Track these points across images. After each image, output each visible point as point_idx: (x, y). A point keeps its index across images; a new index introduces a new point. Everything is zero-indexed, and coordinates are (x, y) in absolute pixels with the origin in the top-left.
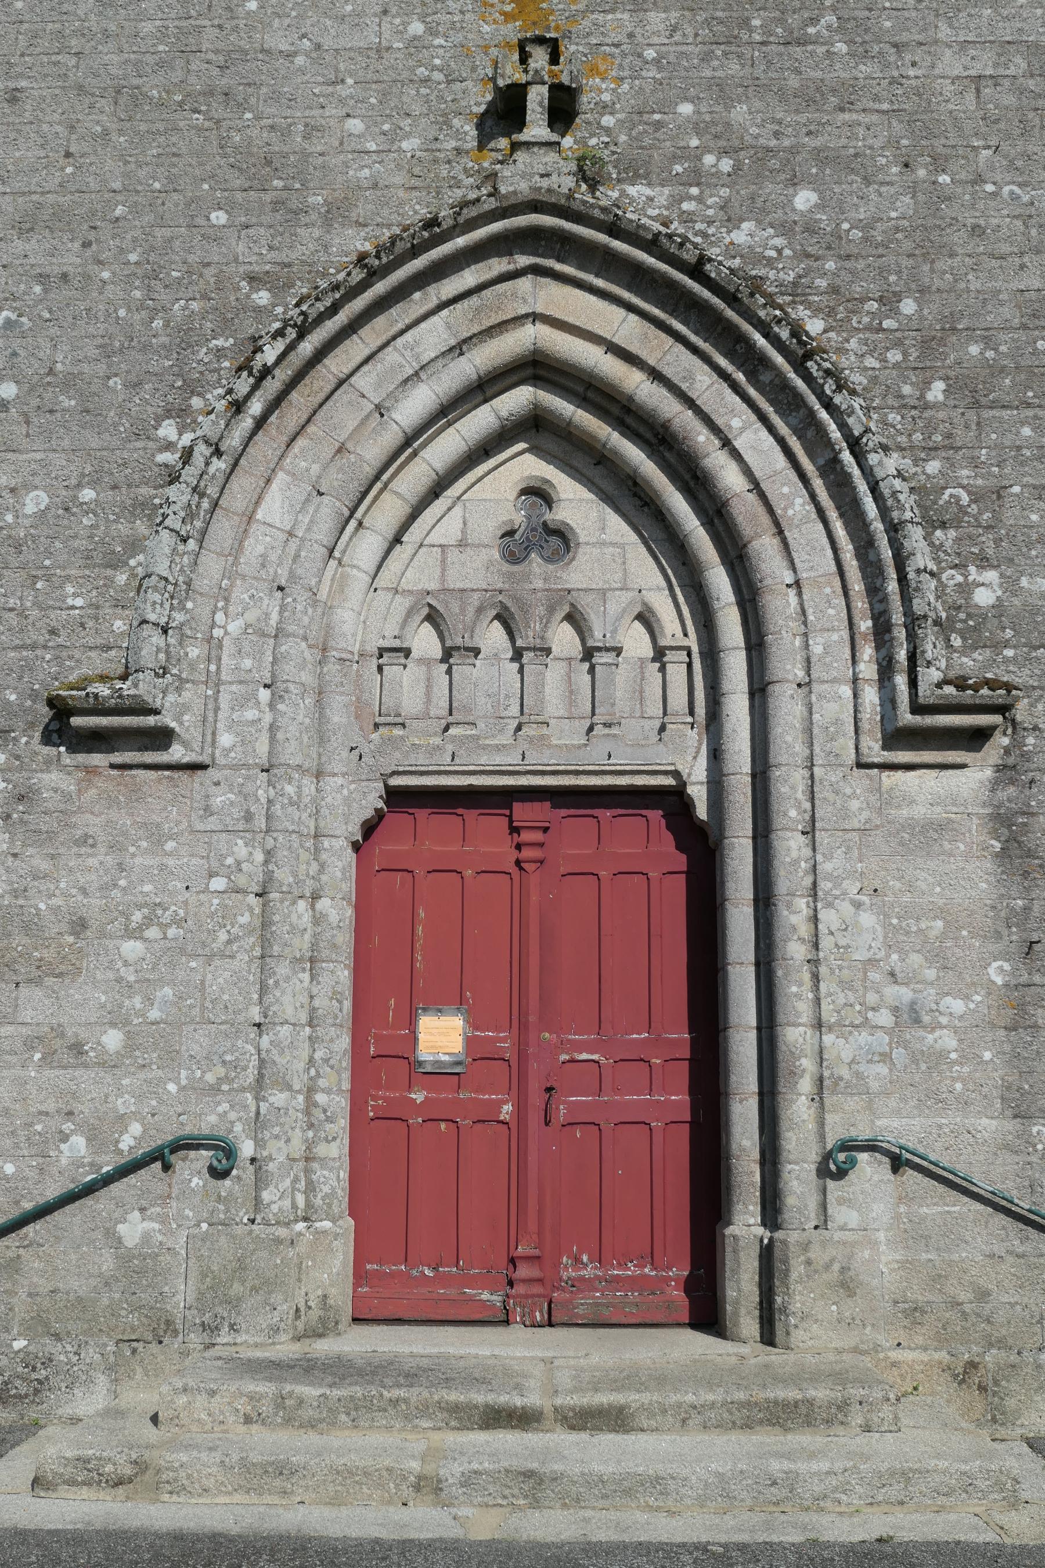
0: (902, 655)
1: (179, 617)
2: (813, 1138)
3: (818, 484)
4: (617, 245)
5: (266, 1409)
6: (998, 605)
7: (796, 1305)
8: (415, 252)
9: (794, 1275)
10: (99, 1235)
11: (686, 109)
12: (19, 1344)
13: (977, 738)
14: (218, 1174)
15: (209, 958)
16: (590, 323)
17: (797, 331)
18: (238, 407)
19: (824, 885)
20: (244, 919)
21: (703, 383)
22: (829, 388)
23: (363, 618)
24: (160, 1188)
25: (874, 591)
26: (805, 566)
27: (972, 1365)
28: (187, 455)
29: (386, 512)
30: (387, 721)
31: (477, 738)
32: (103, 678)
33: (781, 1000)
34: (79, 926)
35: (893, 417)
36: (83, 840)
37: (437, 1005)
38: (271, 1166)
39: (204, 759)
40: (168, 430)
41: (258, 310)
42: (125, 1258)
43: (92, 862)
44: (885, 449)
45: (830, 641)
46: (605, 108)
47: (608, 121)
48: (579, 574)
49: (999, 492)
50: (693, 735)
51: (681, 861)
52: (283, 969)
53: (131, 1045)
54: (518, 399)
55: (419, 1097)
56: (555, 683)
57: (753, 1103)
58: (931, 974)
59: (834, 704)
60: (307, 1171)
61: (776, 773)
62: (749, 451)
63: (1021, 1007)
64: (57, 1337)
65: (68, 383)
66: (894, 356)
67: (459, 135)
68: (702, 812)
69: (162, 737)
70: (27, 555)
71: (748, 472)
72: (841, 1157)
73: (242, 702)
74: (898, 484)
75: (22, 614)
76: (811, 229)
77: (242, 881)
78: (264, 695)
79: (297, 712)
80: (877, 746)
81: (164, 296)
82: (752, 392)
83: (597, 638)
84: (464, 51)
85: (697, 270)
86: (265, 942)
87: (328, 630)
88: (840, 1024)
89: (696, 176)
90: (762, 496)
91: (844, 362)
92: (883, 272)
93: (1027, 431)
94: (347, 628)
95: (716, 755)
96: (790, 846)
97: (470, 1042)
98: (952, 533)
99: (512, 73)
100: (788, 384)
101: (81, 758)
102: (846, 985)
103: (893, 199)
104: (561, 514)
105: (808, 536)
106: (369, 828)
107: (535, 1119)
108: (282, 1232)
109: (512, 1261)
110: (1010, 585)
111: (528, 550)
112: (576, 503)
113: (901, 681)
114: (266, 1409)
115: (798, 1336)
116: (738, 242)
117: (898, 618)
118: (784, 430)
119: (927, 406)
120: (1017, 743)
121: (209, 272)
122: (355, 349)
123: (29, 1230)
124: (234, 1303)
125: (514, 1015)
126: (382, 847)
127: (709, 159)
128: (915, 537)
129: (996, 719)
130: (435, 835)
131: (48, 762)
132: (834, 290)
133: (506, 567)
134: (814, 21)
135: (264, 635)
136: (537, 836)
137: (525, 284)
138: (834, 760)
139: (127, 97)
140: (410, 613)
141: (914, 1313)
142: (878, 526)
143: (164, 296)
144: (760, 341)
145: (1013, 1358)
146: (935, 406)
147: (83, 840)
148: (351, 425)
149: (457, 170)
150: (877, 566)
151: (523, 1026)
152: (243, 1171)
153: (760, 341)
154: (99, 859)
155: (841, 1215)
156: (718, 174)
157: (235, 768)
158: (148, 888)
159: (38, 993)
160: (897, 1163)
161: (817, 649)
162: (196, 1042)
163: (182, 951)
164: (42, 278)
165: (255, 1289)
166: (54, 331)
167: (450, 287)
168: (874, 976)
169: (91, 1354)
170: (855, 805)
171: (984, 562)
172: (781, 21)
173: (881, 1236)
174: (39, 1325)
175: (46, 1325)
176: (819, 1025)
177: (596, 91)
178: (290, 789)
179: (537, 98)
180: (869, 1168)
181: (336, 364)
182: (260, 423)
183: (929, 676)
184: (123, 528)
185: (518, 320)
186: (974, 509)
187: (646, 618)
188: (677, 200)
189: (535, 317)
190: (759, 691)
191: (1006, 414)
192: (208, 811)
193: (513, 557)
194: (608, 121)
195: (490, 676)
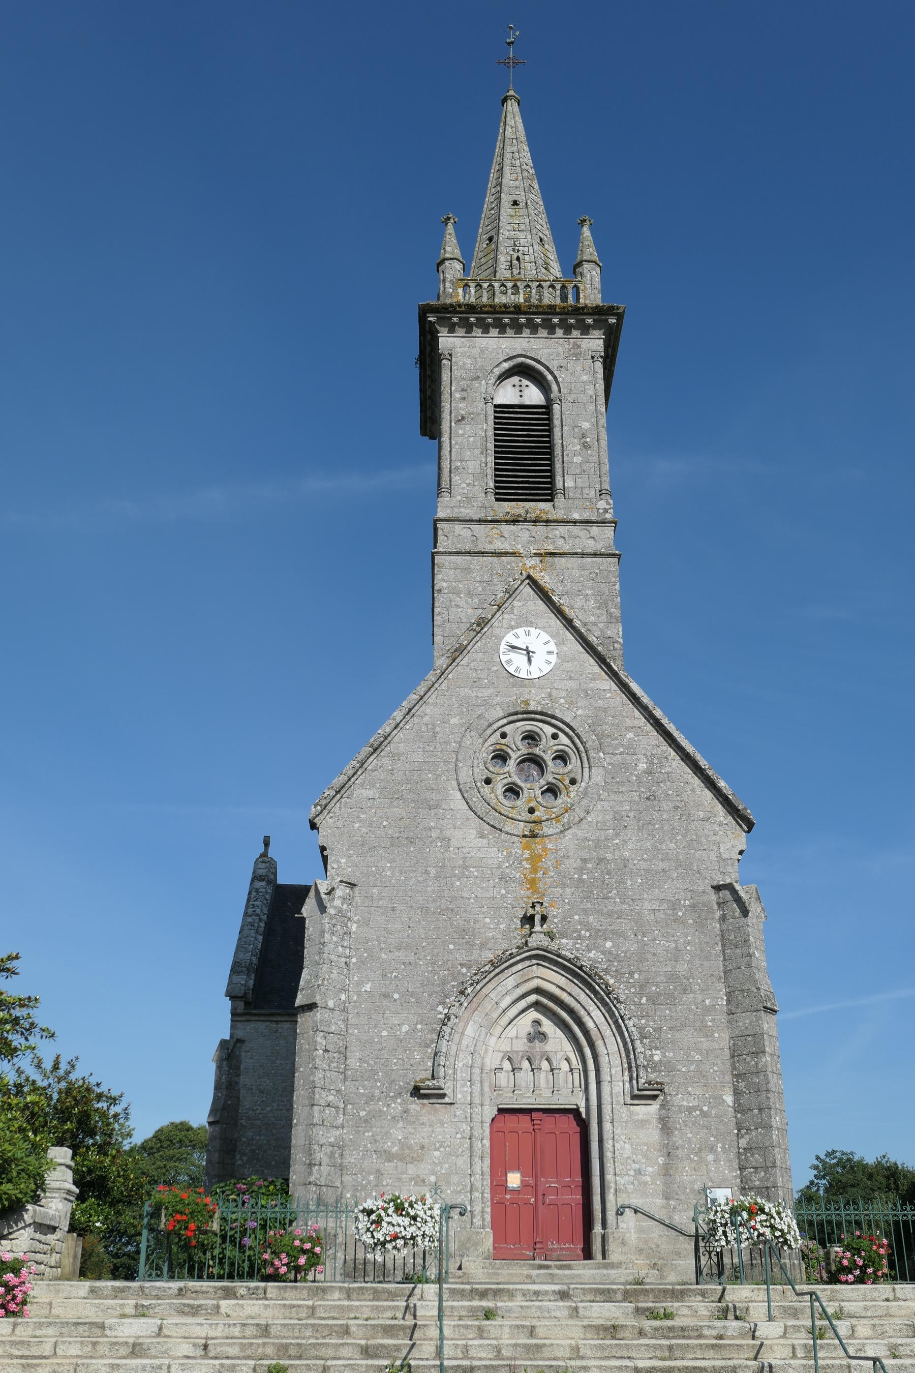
0: (635, 1075)
3: (613, 1026)
4: (560, 960)
7: (611, 1249)
11: (576, 917)
13: (655, 1097)
14: (461, 1214)
16: (553, 980)
17: (607, 985)
19: (616, 1137)
21: (582, 997)
23: (492, 1060)
25: (628, 1056)
33: (605, 1168)
34: (422, 1147)
35: (633, 1007)
40: (440, 1008)
45: (617, 1070)
46: (555, 917)
47: (556, 920)
48: (549, 1047)
49: (660, 1029)
51: (578, 1129)
54: (533, 998)
55: (508, 1197)
56: (543, 1077)
57: (599, 1196)
58: (644, 1161)
59: (618, 1088)
62: (595, 1018)
63: (667, 1170)
66: (633, 990)
68: (584, 1116)
69: (443, 1096)
77: (465, 1135)
78: (469, 1083)
81: (437, 969)
86: (471, 1152)
89: (580, 937)
92: (630, 966)
95: (587, 1100)
96: (607, 1126)
97: (522, 1181)
99: (531, 911)
100: (605, 999)
101: (421, 1101)
102: (622, 1164)
103: (632, 945)
105: (610, 1040)
107: (540, 1203)
109: (535, 1243)
110: (663, 1055)
112: (548, 1026)
113: (634, 1082)
115: (611, 1256)
116: (590, 957)
117: (634, 1065)
118: (604, 1011)
120: (665, 1098)
122: (490, 986)
124: (468, 1249)
125: (533, 1172)
127: (583, 932)
128: (638, 1043)
132: (617, 971)
134: (610, 892)
136: (539, 1122)
137: (535, 967)
138: (618, 1103)
139: (424, 910)
140: (503, 1058)
141: (641, 1251)
142: (628, 1040)
143: (437, 969)
149: (515, 934)
150: (628, 1049)
151: (536, 1176)
152: (468, 1214)
154: (427, 1129)
155: (621, 1225)
160: (636, 1211)
161: (613, 1072)
162: (455, 1179)
164: (404, 963)
167: (515, 969)
170: (624, 1115)
171: (656, 1048)
172: (602, 892)
183: (642, 1081)
185: (533, 978)
188: (574, 944)
189: (537, 977)
190: (598, 1083)
192: (455, 1115)
194: (556, 920)
195: (525, 1076)
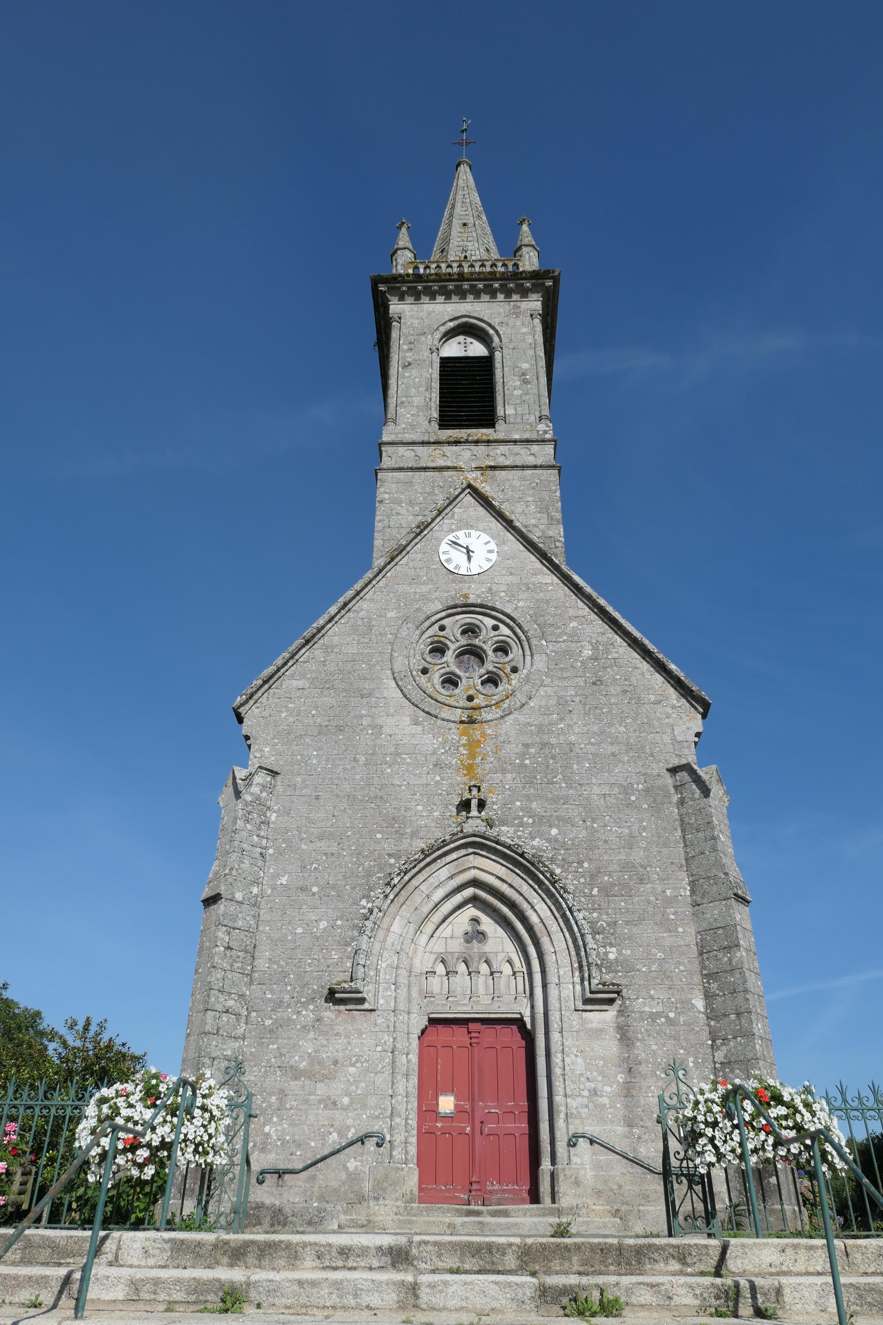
0: (586, 975)
1: (368, 962)
2: (565, 1134)
3: (560, 920)
4: (498, 847)
5: (402, 1210)
6: (616, 959)
7: (561, 1190)
8: (438, 849)
9: (560, 1180)
10: (341, 1167)
11: (518, 803)
12: (315, 1205)
13: (611, 1001)
14: (379, 1145)
15: (376, 1073)
16: (490, 870)
18: (386, 896)
19: (566, 1049)
20: (387, 1060)
21: (525, 888)
22: (562, 892)
23: (422, 961)
24: (361, 1151)
25: (578, 954)
26: (557, 946)
27: (618, 1210)
28: (371, 911)
29: (429, 928)
30: (428, 995)
31: (457, 1001)
32: (345, 982)
33: (554, 1087)
34: (336, 1062)
35: (582, 899)
36: (337, 1034)
37: (445, 1092)
38: (396, 1143)
39: (375, 1008)
40: (364, 902)
41: (391, 865)
42: (349, 1174)
43: (340, 1041)
44: (579, 910)
45: (565, 970)
46: (494, 803)
47: (495, 807)
48: (489, 947)
49: (615, 923)
50: (525, 1000)
51: (523, 1043)
52: (399, 1077)
53: (352, 1102)
54: (469, 892)
55: (439, 1125)
56: (482, 983)
57: (547, 1123)
58: (600, 1078)
60: (406, 1147)
61: (550, 1013)
62: (539, 910)
63: (628, 1089)
64: (328, 1202)
65: (333, 887)
66: (582, 880)
67: (450, 811)
68: (529, 1026)
69: (362, 1001)
70: (320, 942)
71: (539, 916)
72: (574, 1140)
73: (386, 990)
74: (583, 922)
75: (319, 961)
76: (556, 841)
77: (386, 1048)
78: (393, 987)
79: (403, 992)
80: (581, 1004)
82: (540, 891)
83: (494, 969)
84: (451, 785)
85: (522, 855)
86: (393, 1068)
87: (411, 965)
88: (572, 1095)
89: (522, 824)
90: (544, 924)
91: (567, 882)
92: (578, 854)
93: (623, 904)
94: (417, 965)
95: (532, 1007)
96: (555, 1036)
97: (456, 1106)
98: (601, 936)
100: (550, 889)
101: (337, 1007)
102: (574, 1082)
104: (483, 928)
105: (558, 936)
106: (423, 1032)
107: (477, 1132)
108: (399, 1165)
109: (471, 1183)
110: (619, 952)
111: (472, 939)
112: (487, 924)
113: (586, 983)
114: (402, 1210)
115: (562, 1200)
116: (533, 845)
117: (585, 963)
119: (592, 896)
120: (624, 1003)
121: (376, 853)
122: (421, 877)
123: (319, 1165)
124: (384, 1190)
125: (469, 1096)
126: (427, 1038)
127: (525, 819)
128: (589, 938)
129: (615, 995)
130: (444, 1034)
131: (326, 1009)
132: (564, 859)
133: (466, 945)
134: (555, 777)
135: (392, 968)
137: (471, 857)
138: (568, 1010)
141: (599, 1193)
142: (578, 935)
143: (362, 860)
144: (541, 877)
145: (631, 1208)
146: (595, 896)
147: (337, 1034)
148: (419, 901)
150: (578, 946)
151: (473, 1100)
152: (387, 1145)
153: (541, 877)
154: (342, 1040)
155: (575, 1159)
156: (528, 824)
157: (384, 1011)
158: (357, 1050)
159: (323, 1085)
160: (592, 1142)
161: (562, 973)
162: (372, 1101)
163: (368, 1071)
164: (326, 854)
165: (391, 1185)
166: (329, 871)
168: (582, 1079)
169: (339, 1208)
170: (574, 1023)
171: (611, 945)
172: (546, 777)
173: (588, 1167)
174: (322, 1198)
175: (324, 1198)
176: (566, 1096)
177: (491, 798)
178: (401, 1018)
179: (474, 803)
180: (582, 1143)
181: (414, 882)
182: (392, 901)
183: (595, 982)
184: (350, 933)
185: (469, 868)
186: (608, 928)
187: (510, 962)
189: (474, 867)
190: (545, 986)
191: (616, 898)
193: (468, 941)
194: (495, 807)
195: (461, 980)
